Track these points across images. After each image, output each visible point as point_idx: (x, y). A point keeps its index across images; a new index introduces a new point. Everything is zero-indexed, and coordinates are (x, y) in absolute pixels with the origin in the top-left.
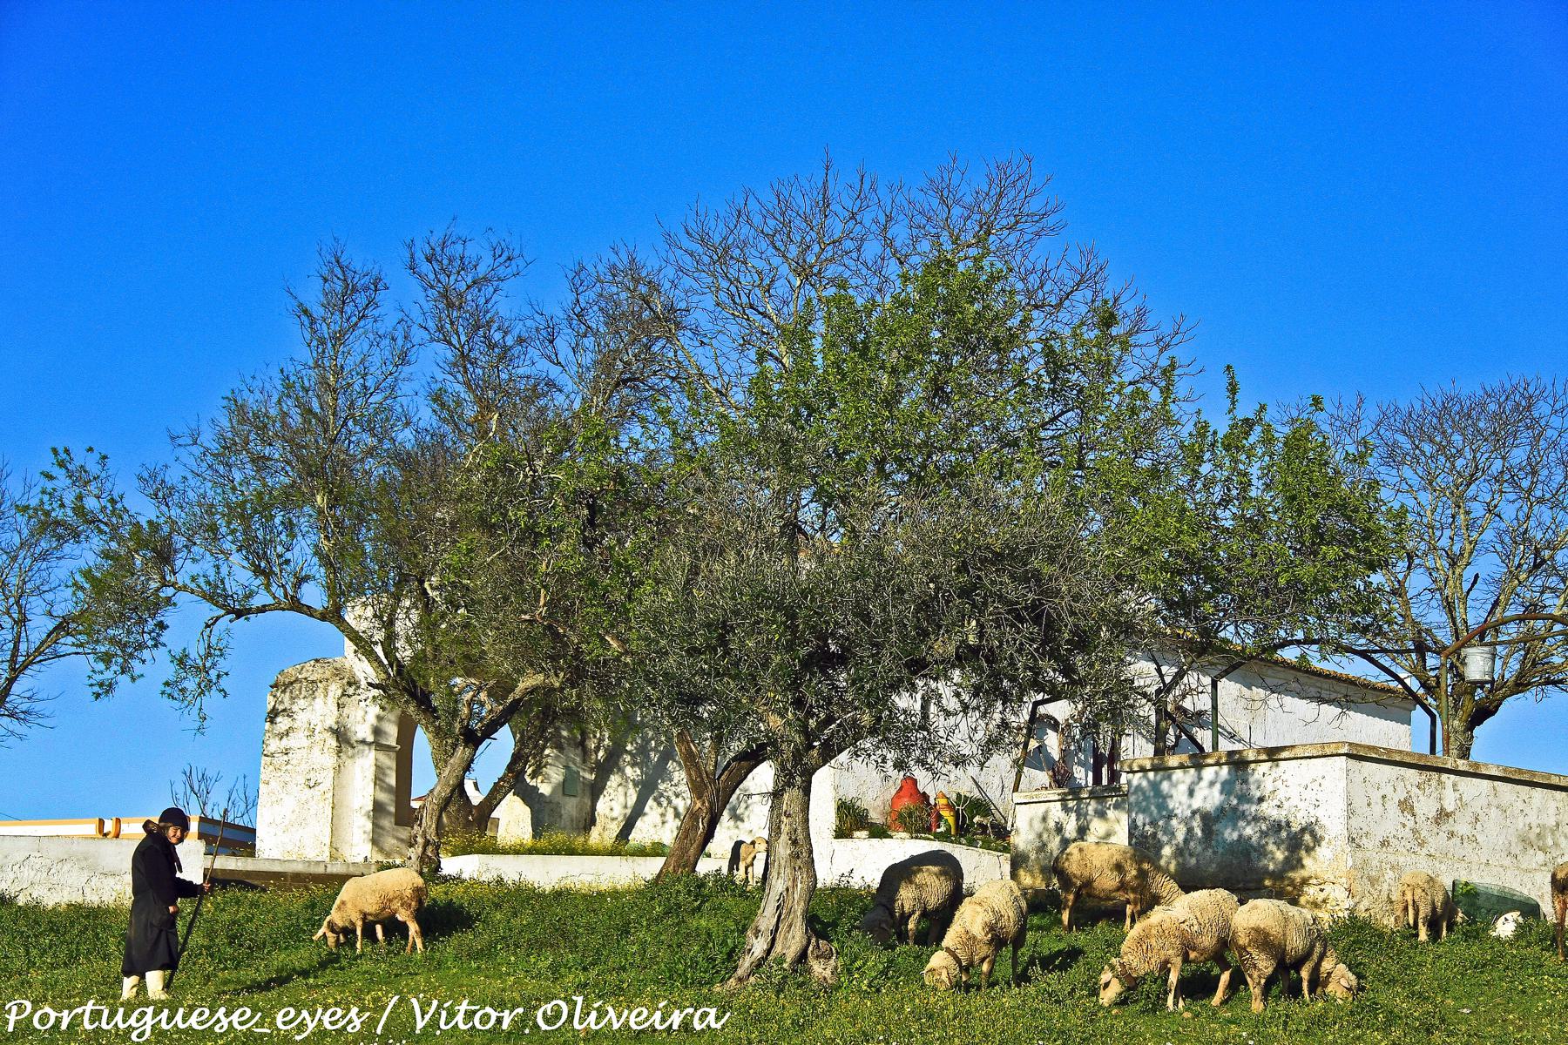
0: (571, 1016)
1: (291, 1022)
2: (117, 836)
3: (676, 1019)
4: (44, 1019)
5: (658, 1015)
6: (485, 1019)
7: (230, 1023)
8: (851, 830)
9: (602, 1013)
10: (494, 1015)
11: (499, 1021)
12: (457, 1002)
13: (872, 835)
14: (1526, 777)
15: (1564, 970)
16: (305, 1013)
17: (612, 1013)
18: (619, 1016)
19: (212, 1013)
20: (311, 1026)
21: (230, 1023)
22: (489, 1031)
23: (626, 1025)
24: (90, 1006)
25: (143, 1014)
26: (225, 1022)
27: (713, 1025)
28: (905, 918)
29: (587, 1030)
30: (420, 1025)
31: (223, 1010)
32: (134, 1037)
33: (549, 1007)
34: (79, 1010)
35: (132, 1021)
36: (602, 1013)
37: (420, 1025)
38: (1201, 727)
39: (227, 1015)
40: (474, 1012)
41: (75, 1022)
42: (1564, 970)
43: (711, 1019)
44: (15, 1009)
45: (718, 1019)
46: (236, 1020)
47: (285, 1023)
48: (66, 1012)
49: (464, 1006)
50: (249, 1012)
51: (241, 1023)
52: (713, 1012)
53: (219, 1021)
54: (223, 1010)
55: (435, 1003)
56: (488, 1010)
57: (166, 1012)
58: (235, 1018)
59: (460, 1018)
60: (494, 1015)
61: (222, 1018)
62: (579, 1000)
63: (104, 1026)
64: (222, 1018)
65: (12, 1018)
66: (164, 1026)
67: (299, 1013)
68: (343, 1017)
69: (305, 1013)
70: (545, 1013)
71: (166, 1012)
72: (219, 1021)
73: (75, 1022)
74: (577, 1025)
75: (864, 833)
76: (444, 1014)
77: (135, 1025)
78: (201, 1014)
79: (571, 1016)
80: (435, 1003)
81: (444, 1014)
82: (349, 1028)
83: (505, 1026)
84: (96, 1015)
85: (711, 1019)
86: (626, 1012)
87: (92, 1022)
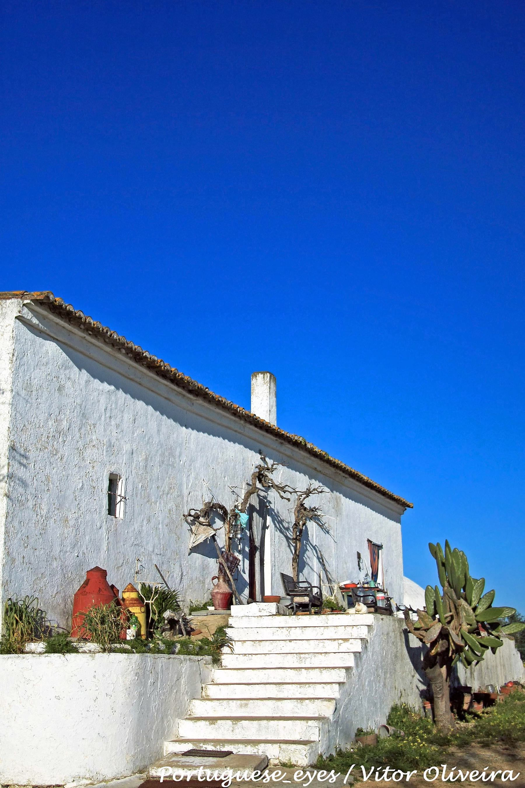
1: (477, 777)
3: (493, 776)
7: (271, 778)
8: (23, 642)
10: (402, 774)
11: (405, 776)
13: (52, 649)
14: (288, 449)
16: (308, 773)
18: (464, 775)
20: (311, 779)
21: (271, 778)
22: (334, 782)
23: (468, 779)
26: (268, 778)
32: (223, 785)
33: (430, 770)
39: (269, 774)
43: (510, 776)
48: (409, 772)
49: (387, 770)
50: (280, 772)
51: (276, 778)
52: (511, 772)
53: (265, 777)
55: (373, 768)
56: (399, 771)
58: (273, 775)
59: (385, 775)
61: (267, 775)
64: (267, 775)
69: (308, 773)
70: (428, 773)
72: (331, 777)
75: (40, 646)
76: (377, 773)
77: (224, 779)
78: (277, 773)
80: (373, 768)
81: (377, 773)
82: (330, 781)
83: (407, 780)
85: (510, 776)
86: (468, 772)
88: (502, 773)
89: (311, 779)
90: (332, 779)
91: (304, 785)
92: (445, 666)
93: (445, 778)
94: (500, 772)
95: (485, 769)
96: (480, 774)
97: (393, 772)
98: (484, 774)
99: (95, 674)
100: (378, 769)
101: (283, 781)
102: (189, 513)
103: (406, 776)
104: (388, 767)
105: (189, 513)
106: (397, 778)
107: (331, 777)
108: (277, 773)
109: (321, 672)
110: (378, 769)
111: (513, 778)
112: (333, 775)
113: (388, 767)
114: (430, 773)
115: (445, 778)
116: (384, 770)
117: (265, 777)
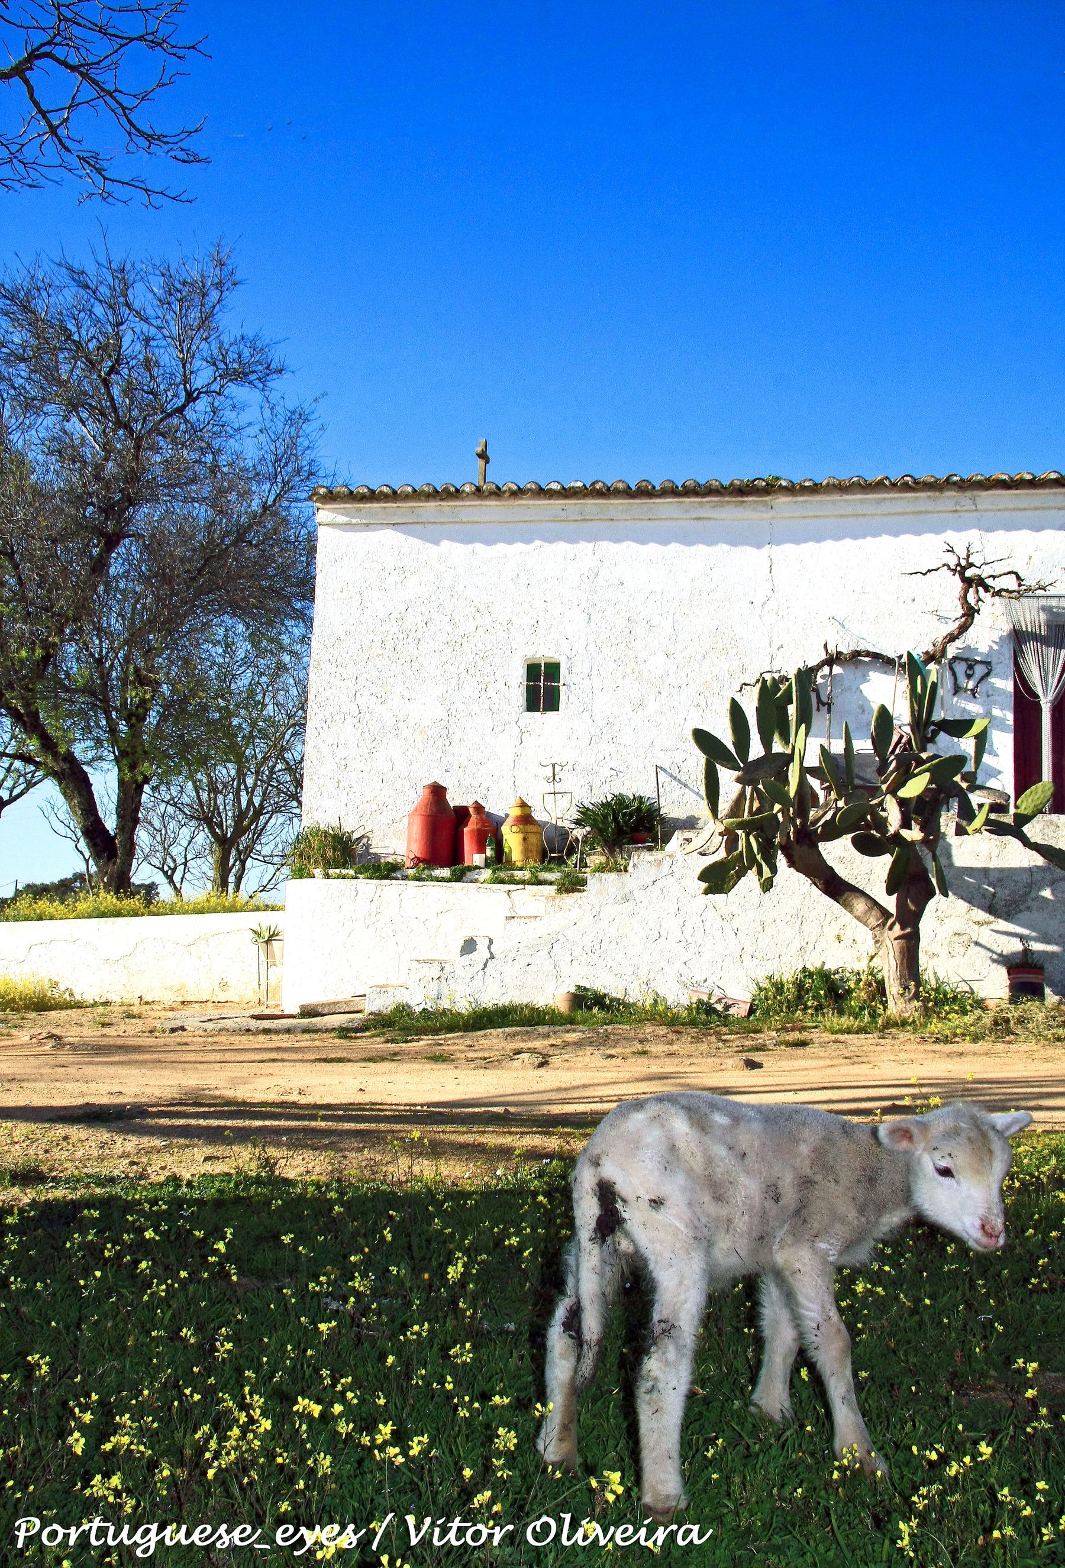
1: (207, 1538)
2: (989, 663)
4: (53, 1535)
5: (643, 1532)
6: (476, 1535)
10: (61, 1531)
11: (67, 1536)
12: (450, 1519)
15: (1062, 1032)
24: (97, 1523)
25: (147, 1531)
26: (226, 1539)
27: (697, 1542)
28: (33, 684)
31: (224, 1527)
33: (538, 1523)
35: (137, 1538)
39: (228, 1532)
40: (467, 1528)
41: (85, 1536)
42: (1062, 1032)
43: (694, 1535)
46: (229, 1537)
47: (242, 1540)
48: (73, 1528)
49: (456, 1523)
50: (631, 1528)
52: (696, 1528)
54: (224, 1527)
58: (236, 1534)
60: (485, 1532)
61: (224, 1534)
62: (567, 1517)
63: (111, 1543)
64: (224, 1534)
65: (22, 1535)
66: (168, 1543)
67: (297, 1531)
70: (535, 1527)
72: (220, 1537)
73: (85, 1536)
76: (437, 1530)
77: (140, 1541)
82: (218, 1545)
83: (71, 1543)
84: (102, 1532)
85: (694, 1535)
87: (98, 1539)
90: (221, 1542)
91: (296, 1553)
92: (895, 895)
93: (684, 1540)
94: (674, 1527)
95: (646, 1522)
96: (636, 1531)
98: (643, 1532)
99: (684, 687)
100: (439, 1522)
101: (256, 1546)
103: (493, 1534)
104: (458, 1519)
106: (473, 1539)
108: (244, 1530)
109: (870, 909)
110: (439, 1522)
111: (700, 1538)
113: (458, 1519)
114: (538, 1529)
115: (684, 1540)
116: (449, 1525)
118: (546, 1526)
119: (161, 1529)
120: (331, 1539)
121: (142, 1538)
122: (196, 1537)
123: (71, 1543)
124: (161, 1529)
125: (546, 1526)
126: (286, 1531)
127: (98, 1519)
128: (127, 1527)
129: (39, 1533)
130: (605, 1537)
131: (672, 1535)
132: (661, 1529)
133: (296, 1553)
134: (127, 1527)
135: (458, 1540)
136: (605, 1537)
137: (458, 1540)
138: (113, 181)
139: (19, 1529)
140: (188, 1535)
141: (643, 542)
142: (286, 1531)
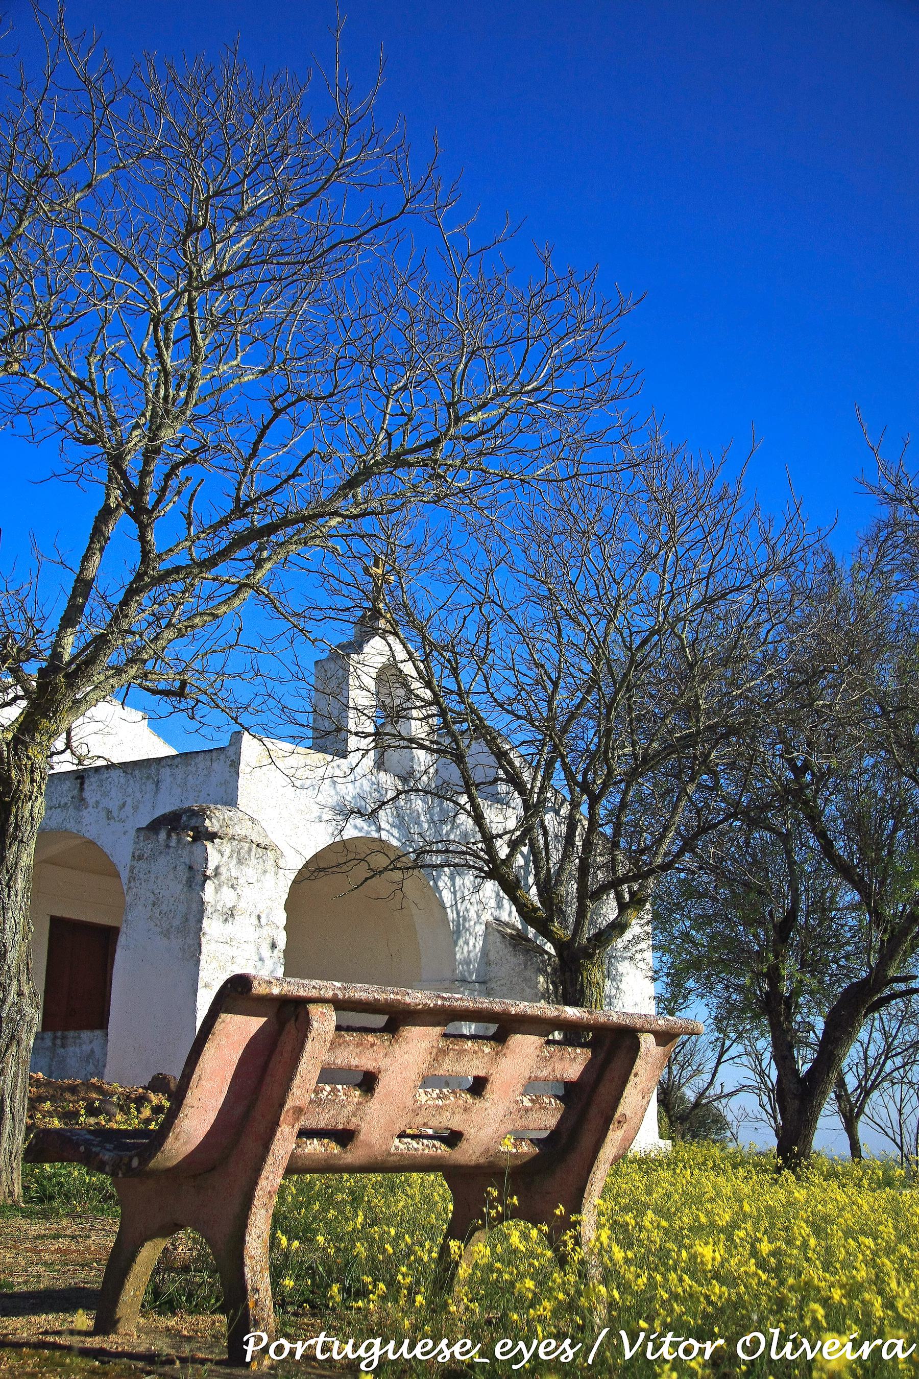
0: (769, 1345)
1: (427, 1353)
7: (452, 1354)
9: (797, 1346)
17: (806, 1344)
18: (812, 1349)
19: (435, 1346)
20: (527, 1356)
21: (452, 1354)
22: (463, 1362)
24: (322, 1338)
26: (447, 1353)
29: (784, 1359)
30: (628, 1355)
31: (445, 1341)
33: (748, 1338)
34: (312, 1342)
35: (361, 1352)
36: (797, 1346)
37: (628, 1355)
38: (656, 916)
39: (449, 1346)
40: (680, 1343)
43: (898, 1349)
44: (252, 1340)
45: (904, 1350)
47: (502, 1354)
48: (300, 1343)
49: (669, 1337)
50: (431, 1343)
51: (462, 1354)
52: (900, 1343)
53: (441, 1351)
54: (445, 1341)
57: (392, 1343)
58: (457, 1349)
61: (568, 1349)
63: (336, 1357)
64: (445, 1349)
66: (391, 1357)
67: (515, 1345)
68: (557, 1348)
69: (521, 1345)
71: (392, 1343)
72: (564, 1351)
74: (774, 1356)
76: (650, 1345)
77: (364, 1355)
78: (464, 1345)
79: (769, 1345)
81: (650, 1345)
82: (440, 1359)
83: (298, 1357)
84: (326, 1348)
88: (883, 1344)
89: (527, 1356)
91: (514, 1367)
97: (681, 1342)
100: (652, 1337)
102: (275, 409)
104: (323, 1334)
105: (275, 409)
107: (564, 1351)
110: (652, 1337)
112: (568, 1349)
113: (323, 1334)
114: (748, 1344)
115: (653, 1354)
117: (441, 1351)
118: (756, 1342)
119: (385, 1342)
120: (836, 1350)
121: (366, 1352)
122: (418, 1351)
123: (298, 1357)
124: (385, 1342)
125: (756, 1342)
126: (504, 1345)
127: (671, 1334)
128: (407, 1342)
129: (267, 1346)
130: (812, 1350)
131: (878, 1349)
132: (867, 1343)
133: (514, 1367)
134: (407, 1342)
135: (409, 1353)
136: (812, 1350)
137: (409, 1353)
138: (367, 879)
139: (247, 1343)
140: (411, 1348)
141: (286, 908)
142: (504, 1345)
